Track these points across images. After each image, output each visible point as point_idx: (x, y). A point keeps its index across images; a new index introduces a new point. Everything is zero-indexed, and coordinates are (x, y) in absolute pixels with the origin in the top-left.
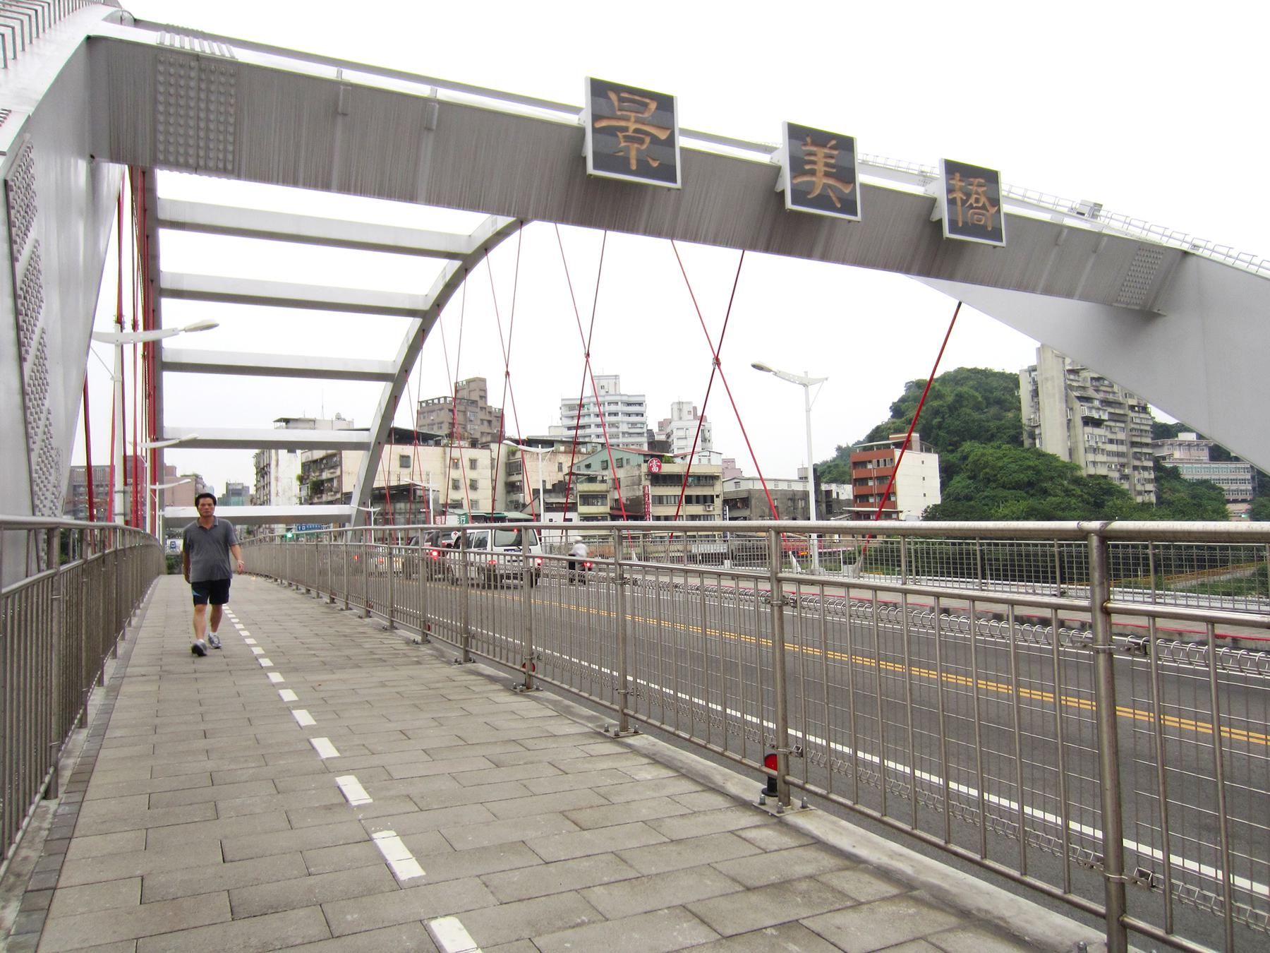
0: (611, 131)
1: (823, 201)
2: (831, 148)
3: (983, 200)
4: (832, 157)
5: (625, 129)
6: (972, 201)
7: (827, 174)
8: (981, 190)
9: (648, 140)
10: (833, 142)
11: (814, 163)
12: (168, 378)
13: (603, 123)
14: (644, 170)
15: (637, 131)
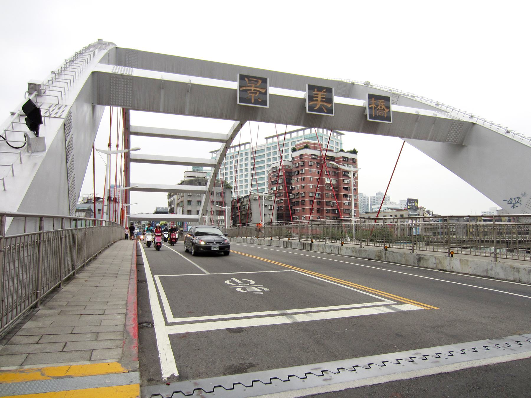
0: (246, 91)
1: (320, 110)
2: (324, 92)
3: (383, 107)
4: (324, 95)
5: (251, 90)
6: (379, 107)
7: (321, 101)
8: (382, 104)
9: (258, 93)
10: (325, 90)
11: (317, 97)
12: (132, 164)
13: (244, 88)
14: (256, 102)
15: (254, 90)
